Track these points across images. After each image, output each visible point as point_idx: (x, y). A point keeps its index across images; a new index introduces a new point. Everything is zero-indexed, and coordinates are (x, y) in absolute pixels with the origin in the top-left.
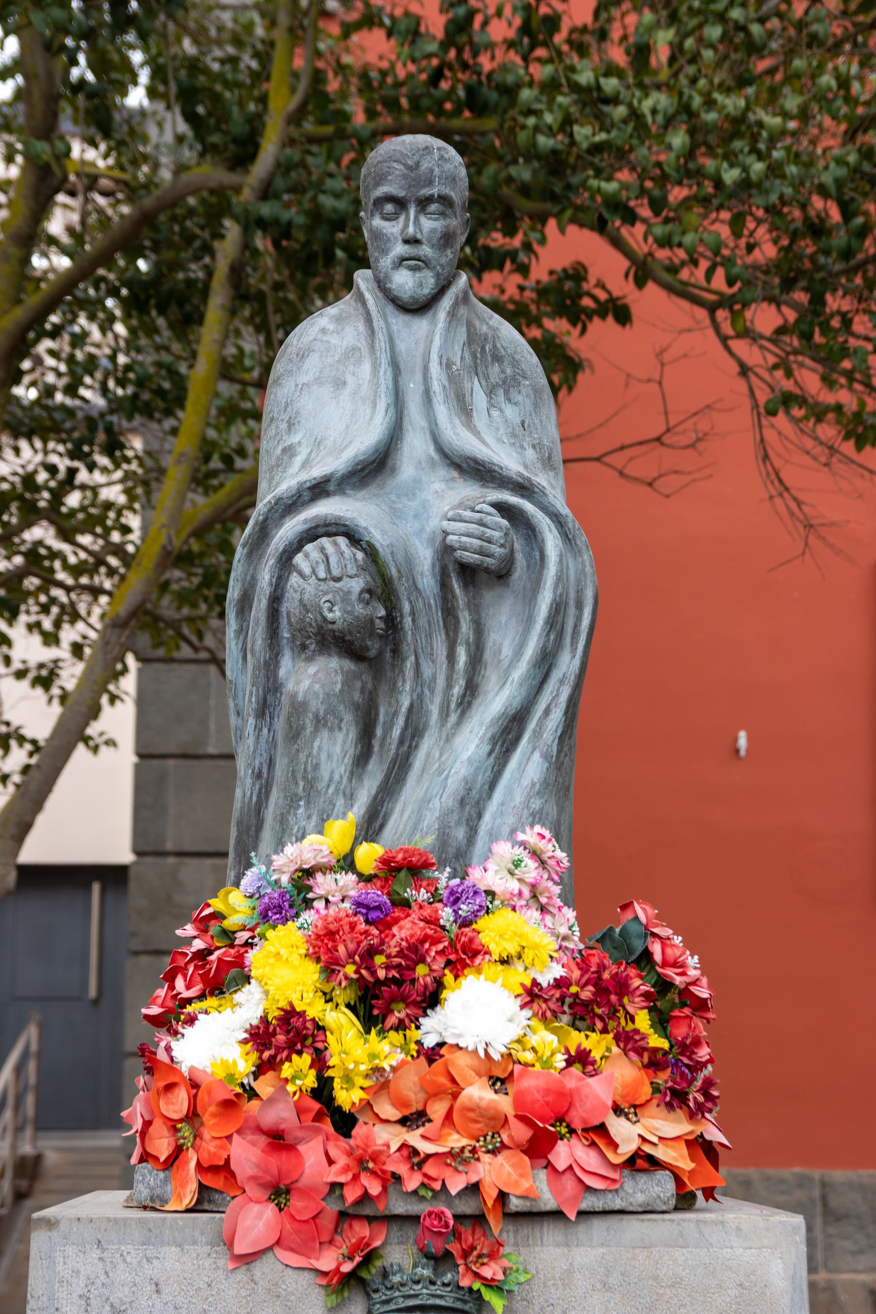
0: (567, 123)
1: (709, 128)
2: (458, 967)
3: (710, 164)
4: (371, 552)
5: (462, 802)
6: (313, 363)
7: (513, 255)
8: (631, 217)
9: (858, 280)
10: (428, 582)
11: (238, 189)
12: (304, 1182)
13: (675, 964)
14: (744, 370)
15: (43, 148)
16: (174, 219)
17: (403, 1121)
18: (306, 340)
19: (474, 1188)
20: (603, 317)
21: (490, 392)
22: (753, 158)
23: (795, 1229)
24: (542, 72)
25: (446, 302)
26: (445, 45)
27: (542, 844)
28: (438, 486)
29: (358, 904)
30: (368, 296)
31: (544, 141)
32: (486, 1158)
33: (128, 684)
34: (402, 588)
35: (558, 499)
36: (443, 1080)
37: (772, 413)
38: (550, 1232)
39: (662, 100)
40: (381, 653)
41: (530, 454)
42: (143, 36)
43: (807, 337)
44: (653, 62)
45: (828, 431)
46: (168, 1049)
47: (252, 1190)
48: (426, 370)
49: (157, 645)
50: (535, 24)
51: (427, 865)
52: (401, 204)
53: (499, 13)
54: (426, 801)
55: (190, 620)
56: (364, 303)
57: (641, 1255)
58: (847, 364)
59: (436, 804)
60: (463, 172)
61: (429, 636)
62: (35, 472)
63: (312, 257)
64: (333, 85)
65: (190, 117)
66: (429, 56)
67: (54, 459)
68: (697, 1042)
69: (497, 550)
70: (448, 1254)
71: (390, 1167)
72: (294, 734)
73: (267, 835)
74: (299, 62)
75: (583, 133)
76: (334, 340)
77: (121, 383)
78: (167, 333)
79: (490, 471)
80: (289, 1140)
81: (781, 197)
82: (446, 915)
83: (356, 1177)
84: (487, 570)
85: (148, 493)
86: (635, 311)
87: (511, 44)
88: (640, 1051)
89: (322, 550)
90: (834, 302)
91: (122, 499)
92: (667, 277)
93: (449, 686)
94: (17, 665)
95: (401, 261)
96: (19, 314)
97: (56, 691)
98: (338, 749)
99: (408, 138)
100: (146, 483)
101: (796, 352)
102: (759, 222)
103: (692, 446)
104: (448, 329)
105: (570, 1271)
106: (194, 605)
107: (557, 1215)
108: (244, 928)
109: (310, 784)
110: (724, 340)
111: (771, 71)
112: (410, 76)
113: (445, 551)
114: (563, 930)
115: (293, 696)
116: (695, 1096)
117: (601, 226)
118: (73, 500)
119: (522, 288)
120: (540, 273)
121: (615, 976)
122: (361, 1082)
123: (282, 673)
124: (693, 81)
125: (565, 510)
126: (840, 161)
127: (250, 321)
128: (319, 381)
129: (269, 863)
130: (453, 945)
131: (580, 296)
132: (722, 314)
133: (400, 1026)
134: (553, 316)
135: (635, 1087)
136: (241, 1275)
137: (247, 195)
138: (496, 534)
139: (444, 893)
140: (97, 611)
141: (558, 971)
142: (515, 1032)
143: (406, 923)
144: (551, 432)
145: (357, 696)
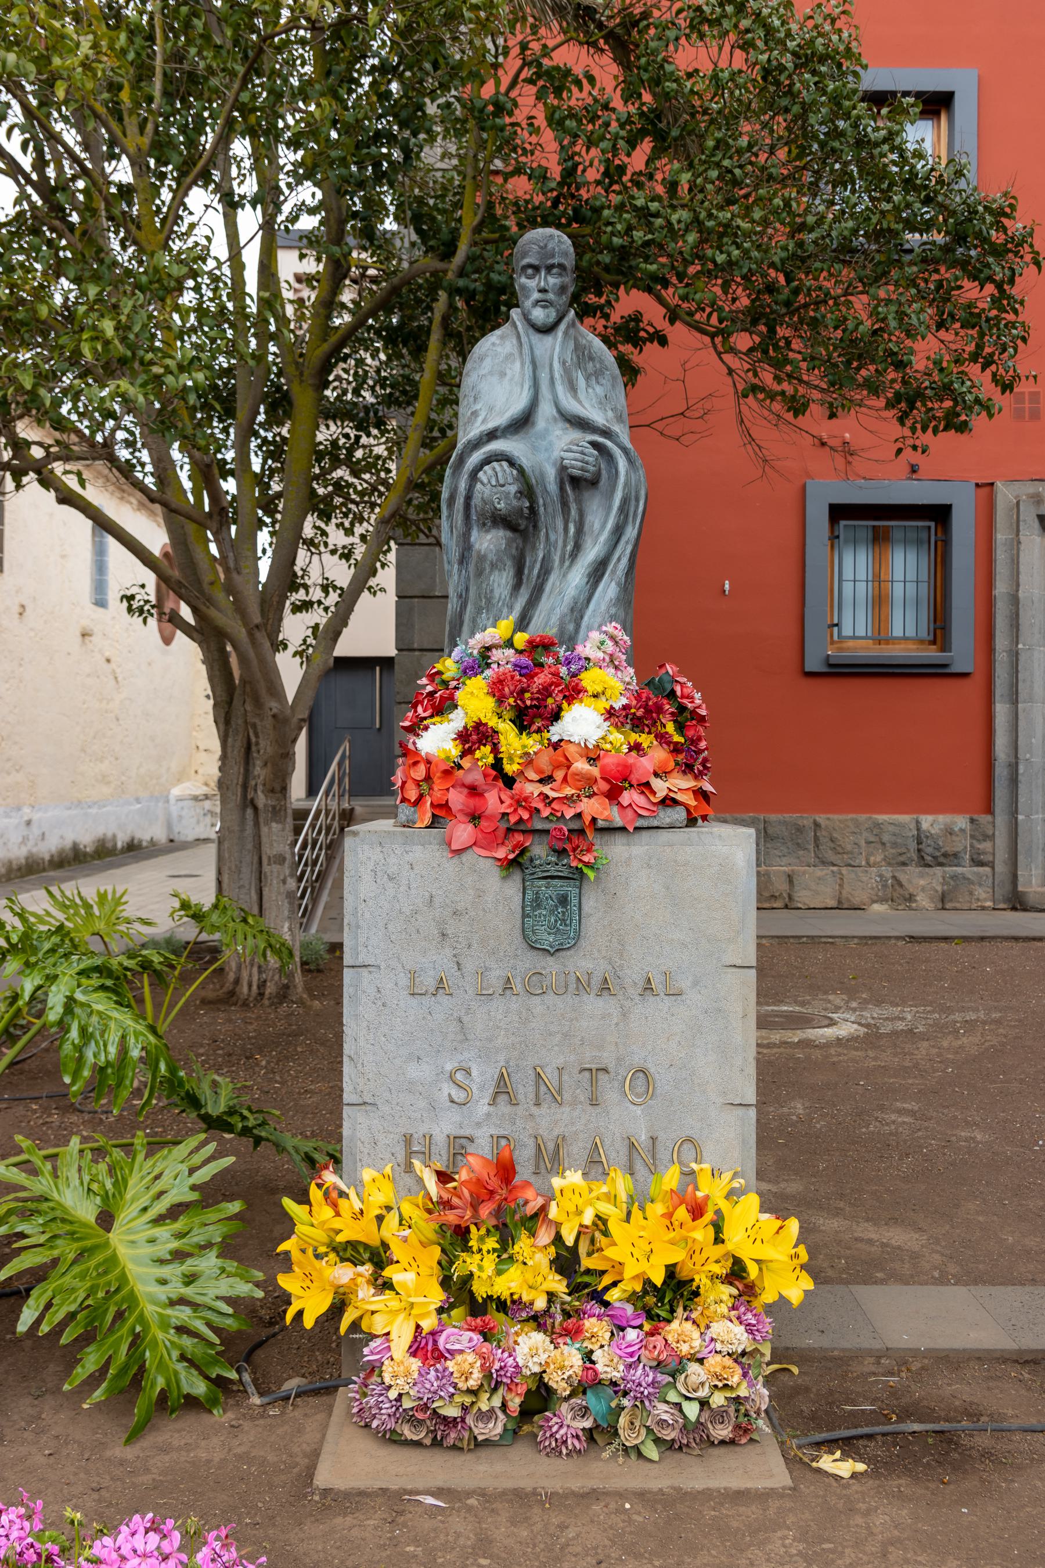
0: (630, 229)
1: (710, 231)
2: (570, 699)
3: (709, 252)
4: (521, 471)
5: (572, 610)
6: (487, 363)
7: (601, 307)
8: (665, 283)
9: (795, 319)
10: (553, 487)
11: (445, 272)
12: (488, 812)
13: (688, 697)
14: (731, 371)
15: (336, 249)
16: (410, 291)
17: (541, 781)
18: (483, 349)
19: (579, 816)
20: (652, 342)
21: (587, 378)
22: (734, 247)
23: (750, 836)
24: (616, 199)
25: (562, 326)
26: (560, 184)
27: (616, 632)
28: (558, 432)
29: (516, 665)
30: (518, 323)
31: (617, 241)
32: (585, 800)
33: (392, 557)
34: (538, 491)
35: (625, 439)
36: (562, 759)
37: (745, 396)
38: (619, 839)
39: (684, 214)
40: (527, 527)
41: (610, 414)
42: (391, 186)
43: (765, 352)
44: (680, 193)
45: (777, 406)
46: (414, 743)
47: (460, 817)
48: (551, 365)
49: (406, 536)
50: (612, 170)
51: (553, 644)
52: (536, 269)
53: (591, 165)
54: (553, 609)
55: (424, 520)
56: (516, 327)
57: (668, 850)
58: (789, 368)
59: (558, 611)
60: (572, 249)
61: (554, 517)
62: (338, 439)
63: (487, 310)
64: (499, 211)
65: (419, 231)
66: (552, 190)
67: (347, 430)
68: (699, 739)
69: (591, 468)
70: (564, 850)
71: (534, 805)
72: (479, 573)
73: (466, 628)
74: (479, 200)
75: (638, 235)
76: (499, 349)
77: (383, 387)
78: (408, 358)
79: (588, 424)
80: (480, 790)
81: (750, 270)
82: (563, 671)
83: (515, 810)
84: (586, 480)
85: (400, 450)
86: (670, 338)
87: (598, 183)
88: (668, 743)
89: (494, 469)
90: (782, 332)
91: (385, 453)
92: (688, 318)
93: (565, 546)
94: (331, 547)
95: (537, 302)
96: (326, 347)
97: (352, 561)
98: (504, 581)
99: (540, 230)
100: (398, 444)
101: (760, 361)
102: (739, 284)
103: (701, 417)
104: (563, 342)
105: (630, 858)
106: (426, 513)
107: (623, 829)
108: (453, 679)
109: (489, 601)
110: (719, 354)
111: (746, 196)
112: (541, 203)
113: (562, 469)
114: (627, 679)
115: (479, 552)
116: (698, 767)
117: (649, 290)
118: (359, 454)
119: (606, 327)
120: (615, 318)
121: (655, 704)
122: (518, 760)
123: (472, 539)
124: (703, 202)
125: (629, 446)
126: (785, 248)
127: (453, 349)
128: (491, 373)
129: (467, 643)
130: (567, 687)
131: (639, 331)
132: (718, 340)
133: (539, 731)
134: (622, 343)
135: (665, 762)
136: (456, 860)
137: (450, 275)
138: (591, 459)
139: (562, 659)
140: (373, 517)
141: (624, 701)
142: (600, 733)
143: (542, 676)
144: (621, 400)
145: (514, 551)
